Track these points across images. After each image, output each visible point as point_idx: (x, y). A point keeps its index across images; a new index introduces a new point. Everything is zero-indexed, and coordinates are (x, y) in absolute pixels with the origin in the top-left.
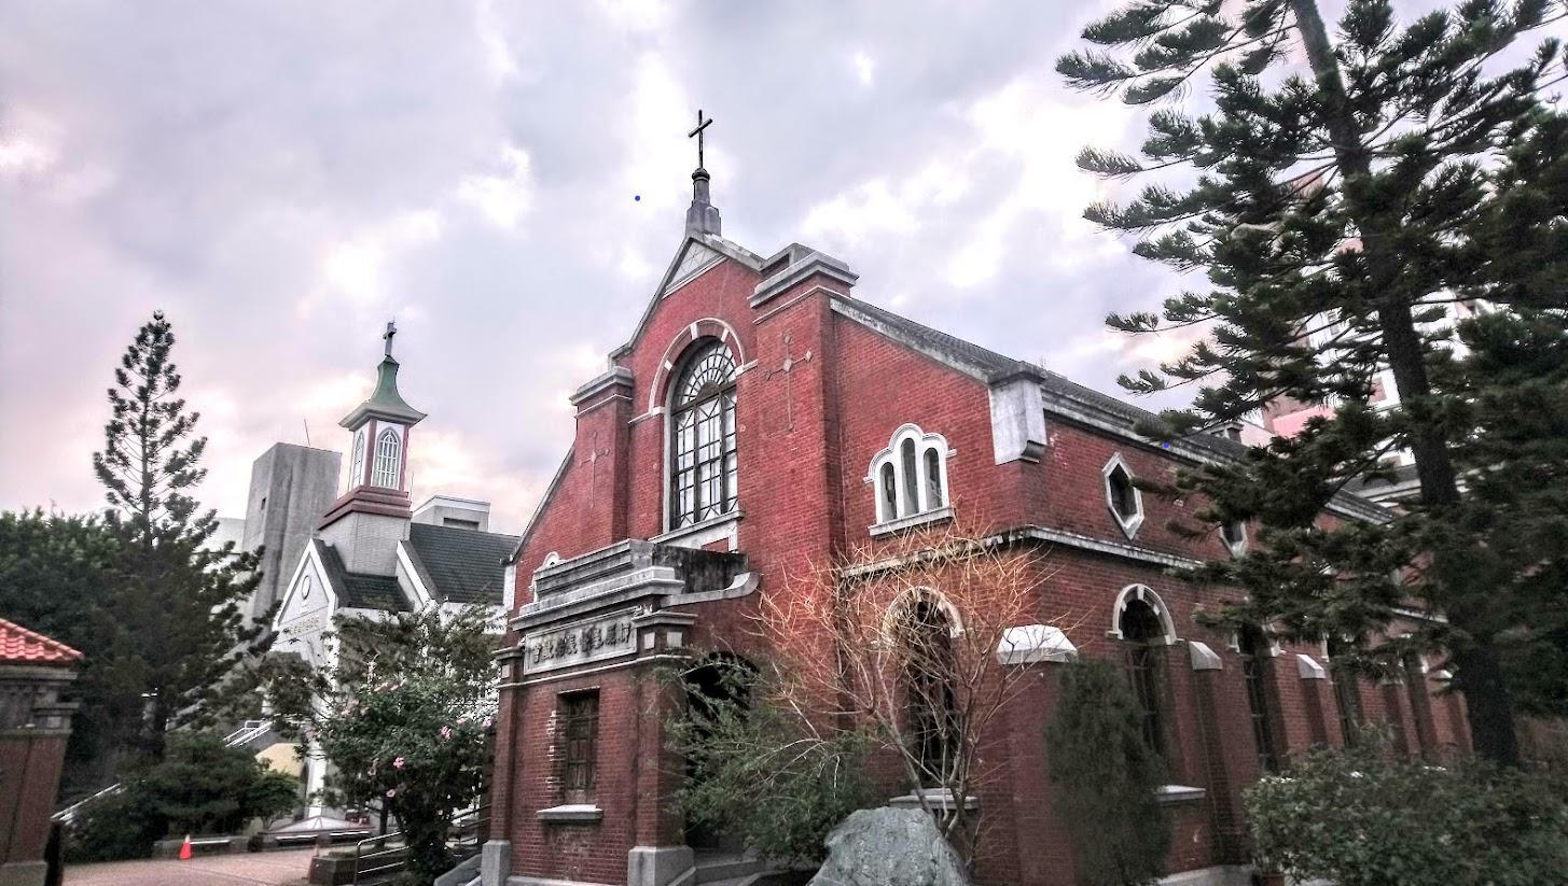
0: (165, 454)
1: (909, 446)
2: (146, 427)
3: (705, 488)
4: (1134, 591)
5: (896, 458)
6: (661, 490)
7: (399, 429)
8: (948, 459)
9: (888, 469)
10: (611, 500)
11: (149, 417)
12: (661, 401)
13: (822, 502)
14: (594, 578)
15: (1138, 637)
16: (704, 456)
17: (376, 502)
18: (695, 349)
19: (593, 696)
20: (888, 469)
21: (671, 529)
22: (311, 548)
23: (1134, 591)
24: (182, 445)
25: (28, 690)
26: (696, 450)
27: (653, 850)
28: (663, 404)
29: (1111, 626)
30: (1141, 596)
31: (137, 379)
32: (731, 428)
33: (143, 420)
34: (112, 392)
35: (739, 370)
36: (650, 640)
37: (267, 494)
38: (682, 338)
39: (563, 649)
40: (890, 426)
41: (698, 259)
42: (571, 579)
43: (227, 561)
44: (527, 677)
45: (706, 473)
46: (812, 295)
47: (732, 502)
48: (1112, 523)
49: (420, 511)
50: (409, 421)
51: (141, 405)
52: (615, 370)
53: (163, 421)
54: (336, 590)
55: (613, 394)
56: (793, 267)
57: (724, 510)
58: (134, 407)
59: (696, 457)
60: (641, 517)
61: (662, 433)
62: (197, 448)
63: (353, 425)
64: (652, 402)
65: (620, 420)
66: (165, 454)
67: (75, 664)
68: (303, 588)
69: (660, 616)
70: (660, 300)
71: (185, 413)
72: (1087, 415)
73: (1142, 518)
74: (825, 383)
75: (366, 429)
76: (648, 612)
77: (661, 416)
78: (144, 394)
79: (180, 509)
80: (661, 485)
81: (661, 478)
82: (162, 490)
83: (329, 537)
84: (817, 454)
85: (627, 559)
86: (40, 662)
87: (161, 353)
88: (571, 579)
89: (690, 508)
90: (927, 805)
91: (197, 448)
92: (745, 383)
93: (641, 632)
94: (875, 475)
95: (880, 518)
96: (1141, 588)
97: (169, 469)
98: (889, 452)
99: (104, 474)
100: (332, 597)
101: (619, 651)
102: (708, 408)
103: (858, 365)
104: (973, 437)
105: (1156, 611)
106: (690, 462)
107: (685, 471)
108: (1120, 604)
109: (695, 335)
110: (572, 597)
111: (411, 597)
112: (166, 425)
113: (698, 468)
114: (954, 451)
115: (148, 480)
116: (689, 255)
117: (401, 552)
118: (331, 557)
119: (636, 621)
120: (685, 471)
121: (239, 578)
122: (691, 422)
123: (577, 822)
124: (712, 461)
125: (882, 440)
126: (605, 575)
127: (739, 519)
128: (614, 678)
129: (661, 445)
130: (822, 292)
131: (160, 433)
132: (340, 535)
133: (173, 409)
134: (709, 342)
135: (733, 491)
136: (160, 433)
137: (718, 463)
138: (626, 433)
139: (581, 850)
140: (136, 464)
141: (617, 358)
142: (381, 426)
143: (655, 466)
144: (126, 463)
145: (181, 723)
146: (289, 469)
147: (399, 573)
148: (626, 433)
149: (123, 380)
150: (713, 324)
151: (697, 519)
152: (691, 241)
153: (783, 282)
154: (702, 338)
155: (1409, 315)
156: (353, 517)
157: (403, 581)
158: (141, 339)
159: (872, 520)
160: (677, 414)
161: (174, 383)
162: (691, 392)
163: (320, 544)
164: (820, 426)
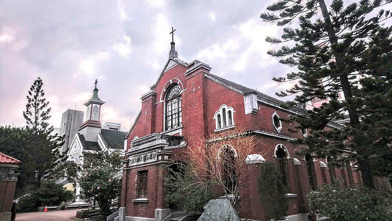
0: (41, 112)
1: (224, 110)
2: (36, 105)
5: (221, 113)
7: (98, 106)
9: (219, 116)
13: (203, 124)
14: (146, 143)
15: (281, 157)
16: (173, 113)
20: (219, 116)
22: (77, 135)
24: (45, 110)
27: (161, 209)
31: (34, 94)
32: (180, 106)
33: (35, 104)
34: (28, 97)
35: (182, 91)
36: (160, 158)
39: (139, 160)
40: (220, 105)
41: (172, 64)
42: (141, 143)
44: (130, 167)
45: (174, 117)
49: (104, 126)
50: (101, 104)
51: (35, 100)
55: (151, 97)
56: (196, 66)
57: (178, 126)
59: (172, 113)
60: (158, 128)
62: (49, 110)
63: (87, 105)
64: (161, 99)
65: (153, 103)
66: (41, 112)
70: (163, 74)
71: (46, 102)
75: (90, 106)
78: (35, 97)
80: (163, 120)
81: (163, 118)
82: (40, 121)
83: (81, 132)
84: (201, 112)
85: (155, 138)
87: (40, 87)
88: (141, 143)
89: (170, 125)
91: (49, 110)
92: (184, 94)
94: (216, 117)
95: (217, 128)
99: (26, 117)
100: (82, 147)
101: (153, 160)
102: (174, 100)
103: (212, 90)
104: (240, 108)
108: (276, 149)
110: (141, 147)
112: (41, 105)
115: (37, 118)
118: (82, 137)
121: (59, 142)
124: (176, 114)
125: (218, 109)
126: (149, 142)
128: (151, 167)
129: (163, 110)
131: (39, 107)
132: (84, 132)
133: (43, 101)
134: (175, 84)
135: (181, 121)
136: (39, 107)
138: (154, 106)
140: (34, 114)
142: (94, 105)
145: (45, 178)
146: (71, 116)
147: (98, 141)
148: (154, 106)
149: (30, 93)
152: (170, 59)
157: (99, 143)
158: (35, 84)
160: (167, 102)
161: (43, 94)
162: (170, 96)
163: (79, 134)
164: (202, 105)
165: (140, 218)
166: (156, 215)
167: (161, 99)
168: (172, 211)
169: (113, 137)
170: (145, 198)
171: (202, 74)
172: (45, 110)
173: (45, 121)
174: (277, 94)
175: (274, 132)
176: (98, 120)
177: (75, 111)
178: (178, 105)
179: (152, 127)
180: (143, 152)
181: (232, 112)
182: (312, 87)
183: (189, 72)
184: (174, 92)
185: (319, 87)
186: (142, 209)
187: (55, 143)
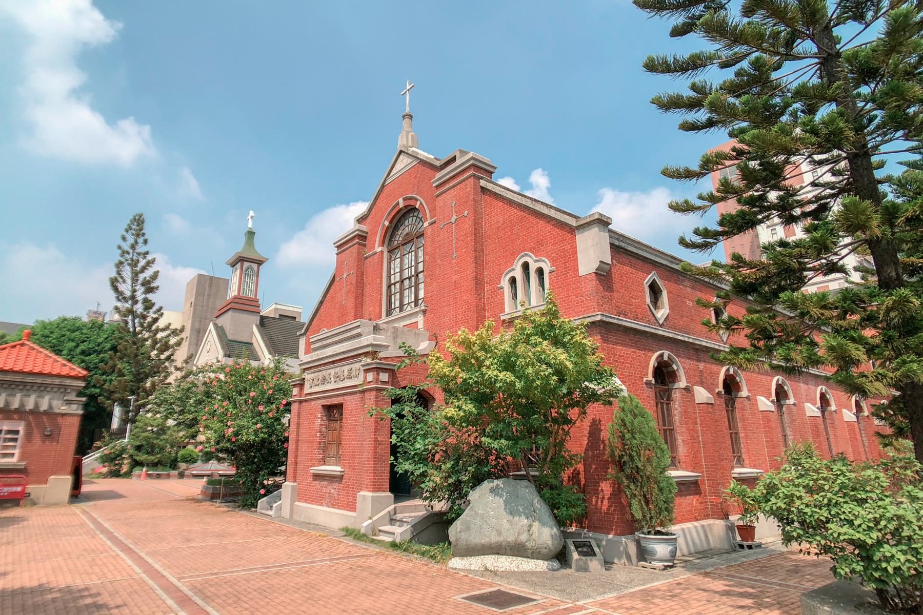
0: (141, 277)
1: (526, 266)
3: (406, 293)
4: (662, 355)
5: (518, 273)
6: (381, 294)
7: (255, 266)
8: (550, 273)
9: (513, 281)
10: (353, 300)
15: (663, 383)
16: (406, 275)
17: (245, 305)
18: (402, 212)
19: (339, 407)
20: (513, 281)
22: (211, 327)
23: (662, 355)
24: (148, 274)
25: (62, 390)
26: (402, 271)
27: (371, 494)
28: (383, 245)
30: (666, 358)
31: (131, 240)
38: (394, 207)
40: (514, 255)
45: (406, 283)
46: (469, 177)
47: (420, 302)
48: (649, 313)
49: (267, 310)
50: (260, 263)
51: (131, 251)
52: (358, 226)
53: (141, 259)
57: (416, 305)
59: (401, 276)
60: (368, 309)
61: (382, 262)
64: (377, 245)
67: (83, 378)
68: (207, 347)
69: (376, 363)
71: (149, 257)
72: (671, 262)
73: (668, 311)
74: (475, 229)
75: (239, 265)
76: (369, 360)
77: (382, 251)
79: (148, 305)
81: (381, 287)
82: (140, 296)
85: (358, 331)
86: (68, 377)
89: (397, 305)
90: (531, 478)
92: (429, 231)
93: (366, 371)
94: (505, 283)
97: (143, 285)
98: (513, 269)
99: (116, 289)
104: (567, 260)
105: (675, 367)
107: (395, 284)
108: (653, 363)
109: (401, 205)
111: (260, 354)
112: (142, 263)
113: (402, 281)
116: (399, 160)
117: (255, 330)
119: (363, 366)
120: (395, 284)
121: (173, 341)
122: (398, 255)
123: (331, 478)
124: (409, 278)
125: (510, 262)
127: (424, 312)
129: (382, 269)
130: (474, 176)
132: (226, 321)
135: (421, 294)
137: (413, 279)
139: (332, 491)
140: (129, 281)
142: (246, 264)
143: (378, 281)
144: (124, 281)
145: (148, 412)
146: (207, 287)
147: (254, 341)
148: (361, 259)
149: (124, 239)
150: (411, 198)
151: (401, 310)
153: (452, 171)
154: (406, 207)
155: (871, 163)
156: (230, 313)
157: (255, 345)
159: (503, 311)
162: (399, 238)
163: (215, 325)
166: (358, 505)
168: (397, 499)
169: (282, 332)
170: (336, 465)
172: (148, 274)
173: (150, 296)
175: (649, 322)
177: (211, 278)
179: (356, 308)
180: (333, 362)
181: (547, 269)
182: (758, 186)
183: (440, 179)
185: (785, 189)
186: (332, 489)
187: (167, 343)
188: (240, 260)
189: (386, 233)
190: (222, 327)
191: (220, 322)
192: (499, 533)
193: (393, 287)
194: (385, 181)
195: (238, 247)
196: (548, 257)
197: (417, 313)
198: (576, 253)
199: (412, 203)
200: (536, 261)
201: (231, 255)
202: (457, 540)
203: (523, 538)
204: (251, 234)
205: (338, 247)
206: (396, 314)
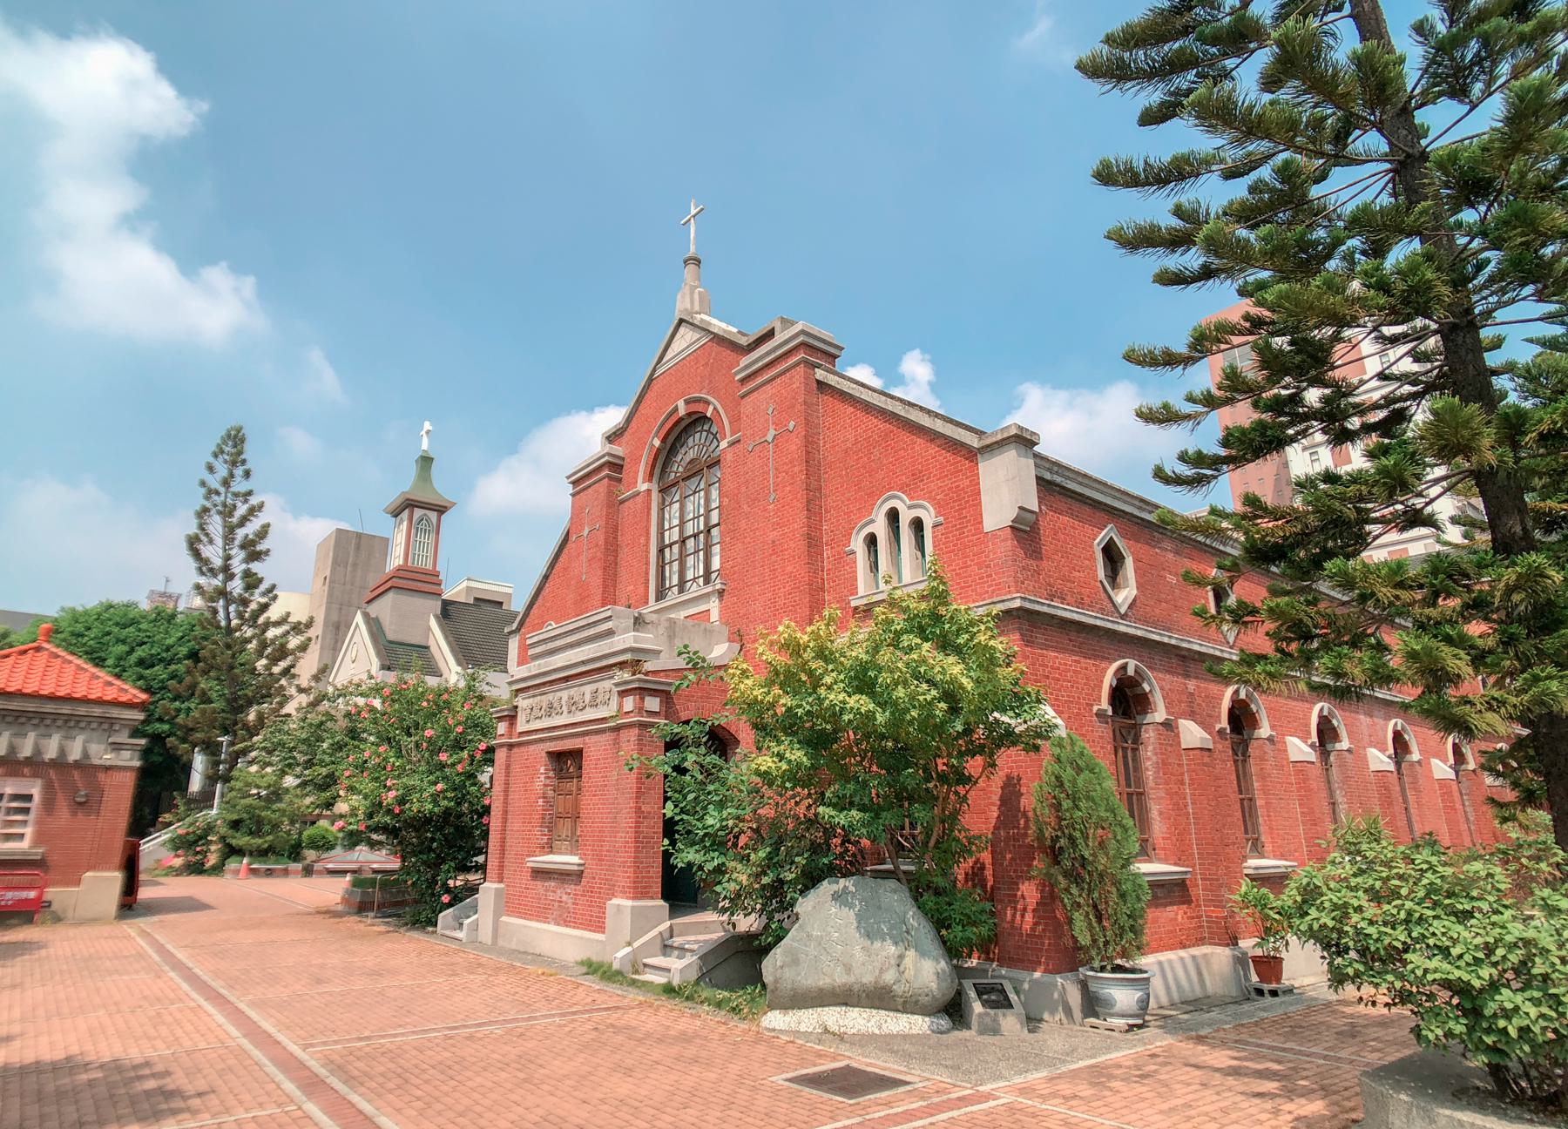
0: (240, 533)
1: (893, 516)
3: (690, 561)
4: (1124, 667)
5: (880, 527)
6: (647, 564)
7: (433, 516)
9: (872, 541)
11: (229, 501)
12: (650, 478)
17: (417, 582)
18: (684, 424)
19: (577, 754)
20: (872, 541)
21: (657, 600)
22: (359, 618)
23: (1124, 667)
24: (251, 529)
25: (106, 726)
26: (682, 523)
27: (630, 903)
28: (650, 480)
29: (1219, 720)
30: (1131, 672)
31: (222, 470)
34: (203, 484)
37: (328, 573)
38: (670, 415)
40: (872, 496)
43: (285, 628)
45: (691, 543)
47: (714, 576)
48: (1103, 595)
49: (454, 590)
50: (441, 510)
51: (222, 490)
53: (1262, 630)
54: (378, 654)
56: (779, 338)
58: (218, 493)
59: (681, 532)
60: (626, 588)
61: (649, 509)
64: (640, 480)
67: (142, 706)
68: (352, 654)
69: (639, 680)
71: (254, 501)
73: (1135, 592)
74: (808, 453)
75: (405, 514)
76: (627, 676)
77: (649, 491)
78: (226, 483)
79: (252, 581)
80: (647, 558)
81: (648, 552)
82: (238, 566)
84: (799, 523)
89: (675, 581)
93: (623, 694)
94: (858, 544)
95: (861, 591)
96: (1132, 665)
97: (242, 547)
98: (872, 521)
104: (963, 505)
105: (1146, 687)
106: (675, 535)
107: (670, 545)
109: (682, 412)
111: (441, 664)
112: (242, 509)
113: (683, 541)
114: (941, 519)
116: (678, 336)
117: (433, 623)
119: (616, 685)
120: (670, 545)
121: (294, 642)
123: (563, 876)
124: (695, 536)
125: (867, 508)
127: (721, 593)
128: (595, 738)
129: (648, 520)
130: (806, 362)
132: (384, 608)
139: (565, 898)
140: (219, 541)
141: (1109, 40)
142: (418, 513)
143: (642, 540)
144: (211, 542)
145: (251, 763)
146: (352, 550)
147: (431, 643)
148: (614, 504)
149: (211, 469)
151: (681, 591)
153: (768, 353)
156: (391, 595)
157: (434, 649)
159: (854, 591)
162: (677, 469)
163: (366, 615)
164: (802, 496)
165: (553, 928)
166: (609, 922)
167: (641, 475)
168: (675, 911)
169: (479, 627)
170: (572, 853)
171: (801, 369)
172: (251, 529)
173: (255, 567)
174: (1159, 474)
175: (1102, 610)
176: (430, 567)
177: (359, 536)
178: (708, 500)
179: (605, 586)
181: (929, 520)
182: (1289, 381)
184: (691, 451)
186: (564, 894)
187: (283, 646)
188: (408, 505)
189: (655, 459)
190: (377, 620)
191: (373, 610)
192: (848, 969)
193: (667, 551)
194: (654, 370)
195: (404, 483)
196: (930, 499)
197: (708, 595)
198: (979, 493)
199: (699, 407)
200: (910, 507)
201: (393, 496)
202: (776, 981)
203: (889, 977)
204: (426, 461)
205: (574, 483)
206: (673, 597)
